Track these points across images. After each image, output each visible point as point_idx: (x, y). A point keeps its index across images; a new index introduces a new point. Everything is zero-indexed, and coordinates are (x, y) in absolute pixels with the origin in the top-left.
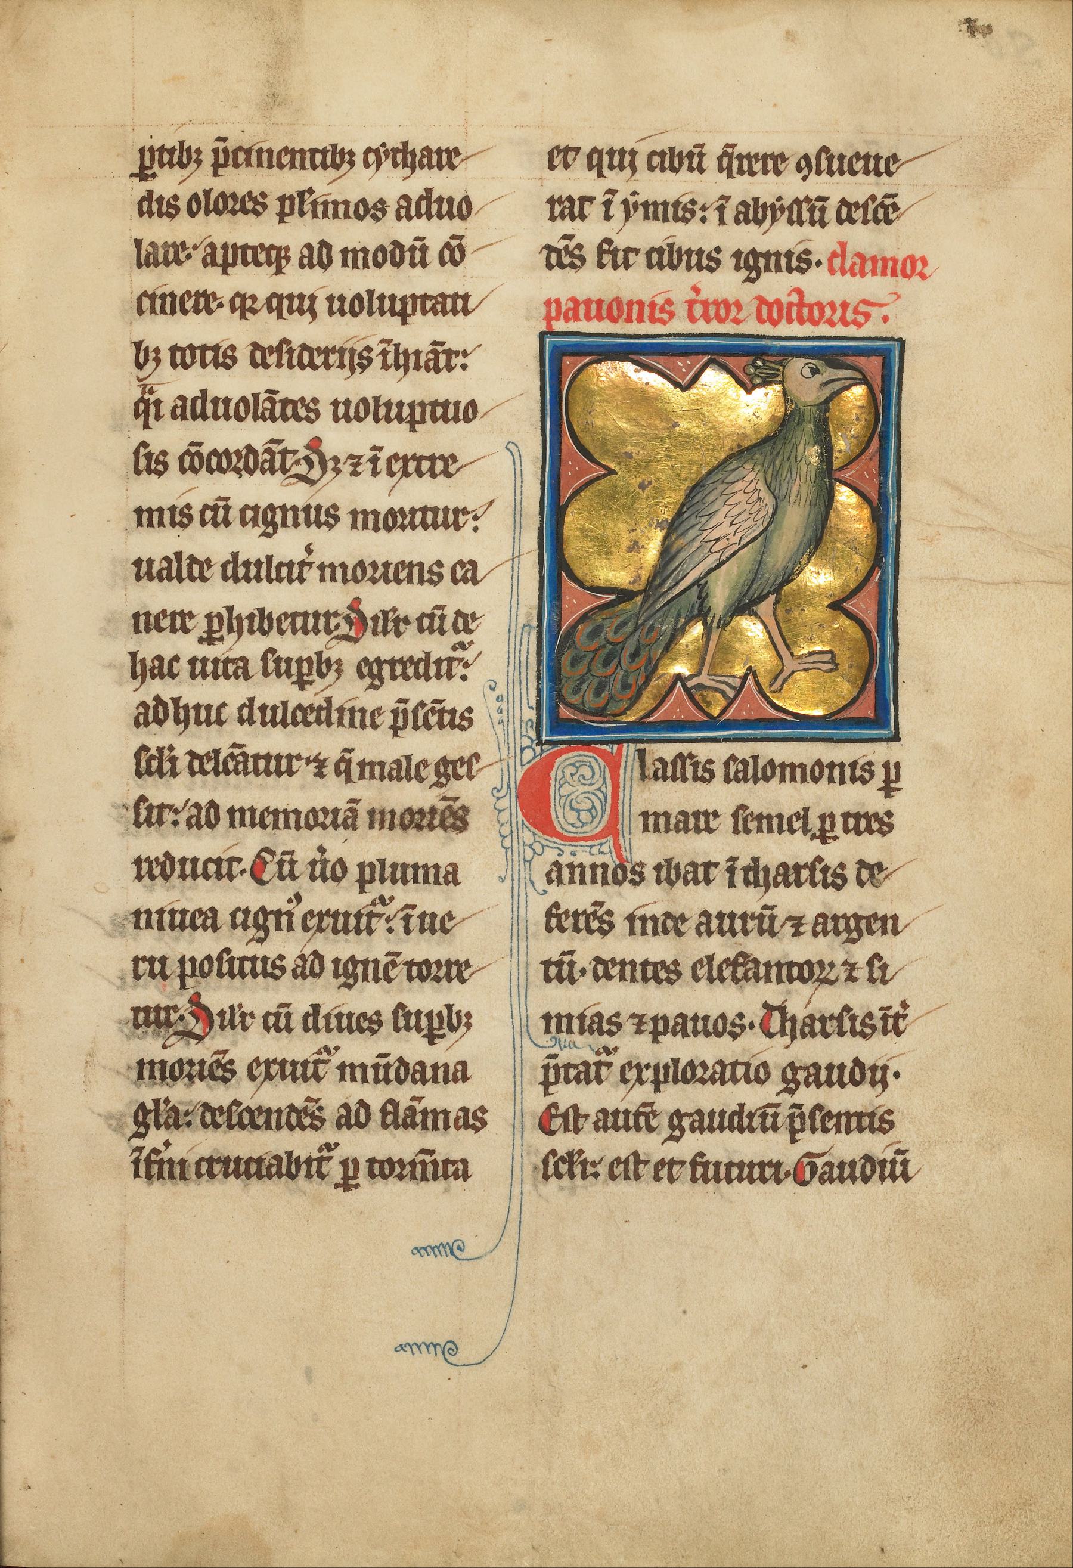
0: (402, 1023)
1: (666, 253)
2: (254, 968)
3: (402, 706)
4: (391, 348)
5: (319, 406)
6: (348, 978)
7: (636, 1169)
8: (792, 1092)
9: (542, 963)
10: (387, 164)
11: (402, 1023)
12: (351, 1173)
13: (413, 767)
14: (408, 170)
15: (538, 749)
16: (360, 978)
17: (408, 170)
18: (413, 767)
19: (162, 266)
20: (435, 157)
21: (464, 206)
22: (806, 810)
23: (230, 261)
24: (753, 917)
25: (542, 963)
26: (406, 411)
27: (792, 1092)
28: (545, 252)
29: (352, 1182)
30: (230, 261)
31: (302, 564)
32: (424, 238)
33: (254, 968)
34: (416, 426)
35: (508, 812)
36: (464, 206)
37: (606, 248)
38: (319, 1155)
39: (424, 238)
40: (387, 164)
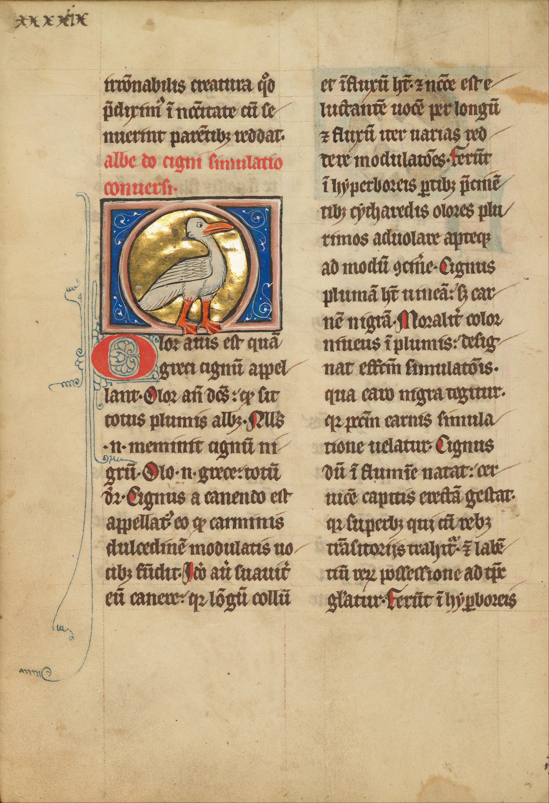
0: (352, 526)
1: (167, 83)
2: (413, 447)
3: (465, 179)
4: (444, 595)
5: (185, 496)
6: (482, 115)
7: (285, 497)
8: (472, 507)
9: (326, 571)
10: (364, 217)
11: (352, 526)
12: (425, 188)
13: (486, 319)
14: (435, 557)
15: (100, 337)
16: (465, 272)
17: (435, 557)
18: (486, 319)
19: (481, 555)
20: (426, 238)
21: (289, 548)
22: (391, 440)
23: (329, 299)
24: (123, 469)
25: (326, 571)
26: (418, 370)
27: (472, 507)
28: (105, 495)
29: (425, 193)
30: (329, 299)
31: (456, 317)
32: (257, 102)
33: (413, 447)
34: (434, 117)
35: (84, 363)
36: (289, 548)
37: (152, 392)
38: (449, 543)
39: (257, 102)
40: (364, 217)
